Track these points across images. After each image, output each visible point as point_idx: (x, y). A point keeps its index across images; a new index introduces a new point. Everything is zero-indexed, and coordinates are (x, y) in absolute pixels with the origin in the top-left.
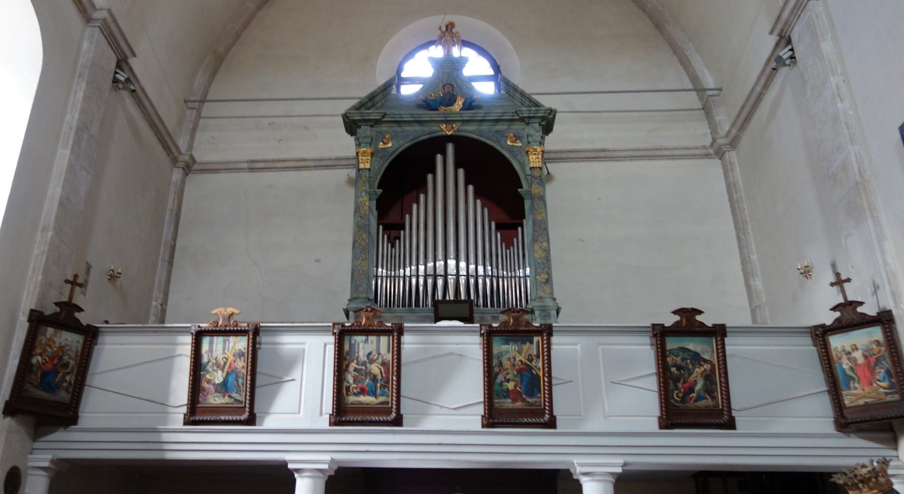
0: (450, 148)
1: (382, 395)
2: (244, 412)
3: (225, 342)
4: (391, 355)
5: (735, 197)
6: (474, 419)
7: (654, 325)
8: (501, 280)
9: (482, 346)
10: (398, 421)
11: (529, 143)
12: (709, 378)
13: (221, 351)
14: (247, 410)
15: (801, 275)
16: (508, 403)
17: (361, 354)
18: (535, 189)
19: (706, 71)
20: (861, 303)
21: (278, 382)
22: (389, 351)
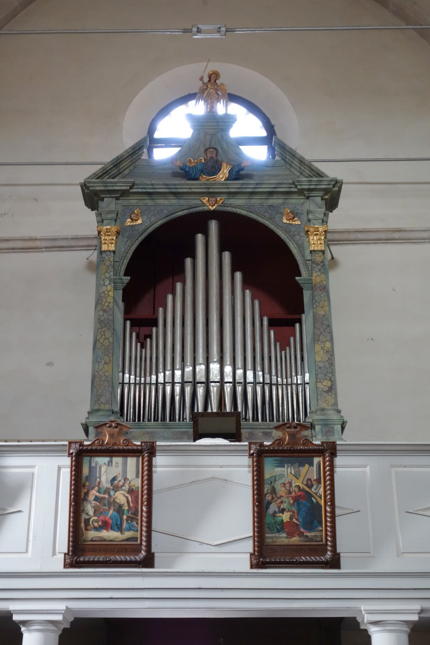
1: (129, 529)
4: (140, 480)
8: (274, 388)
11: (309, 220)
17: (103, 479)
18: (317, 278)
22: (137, 476)
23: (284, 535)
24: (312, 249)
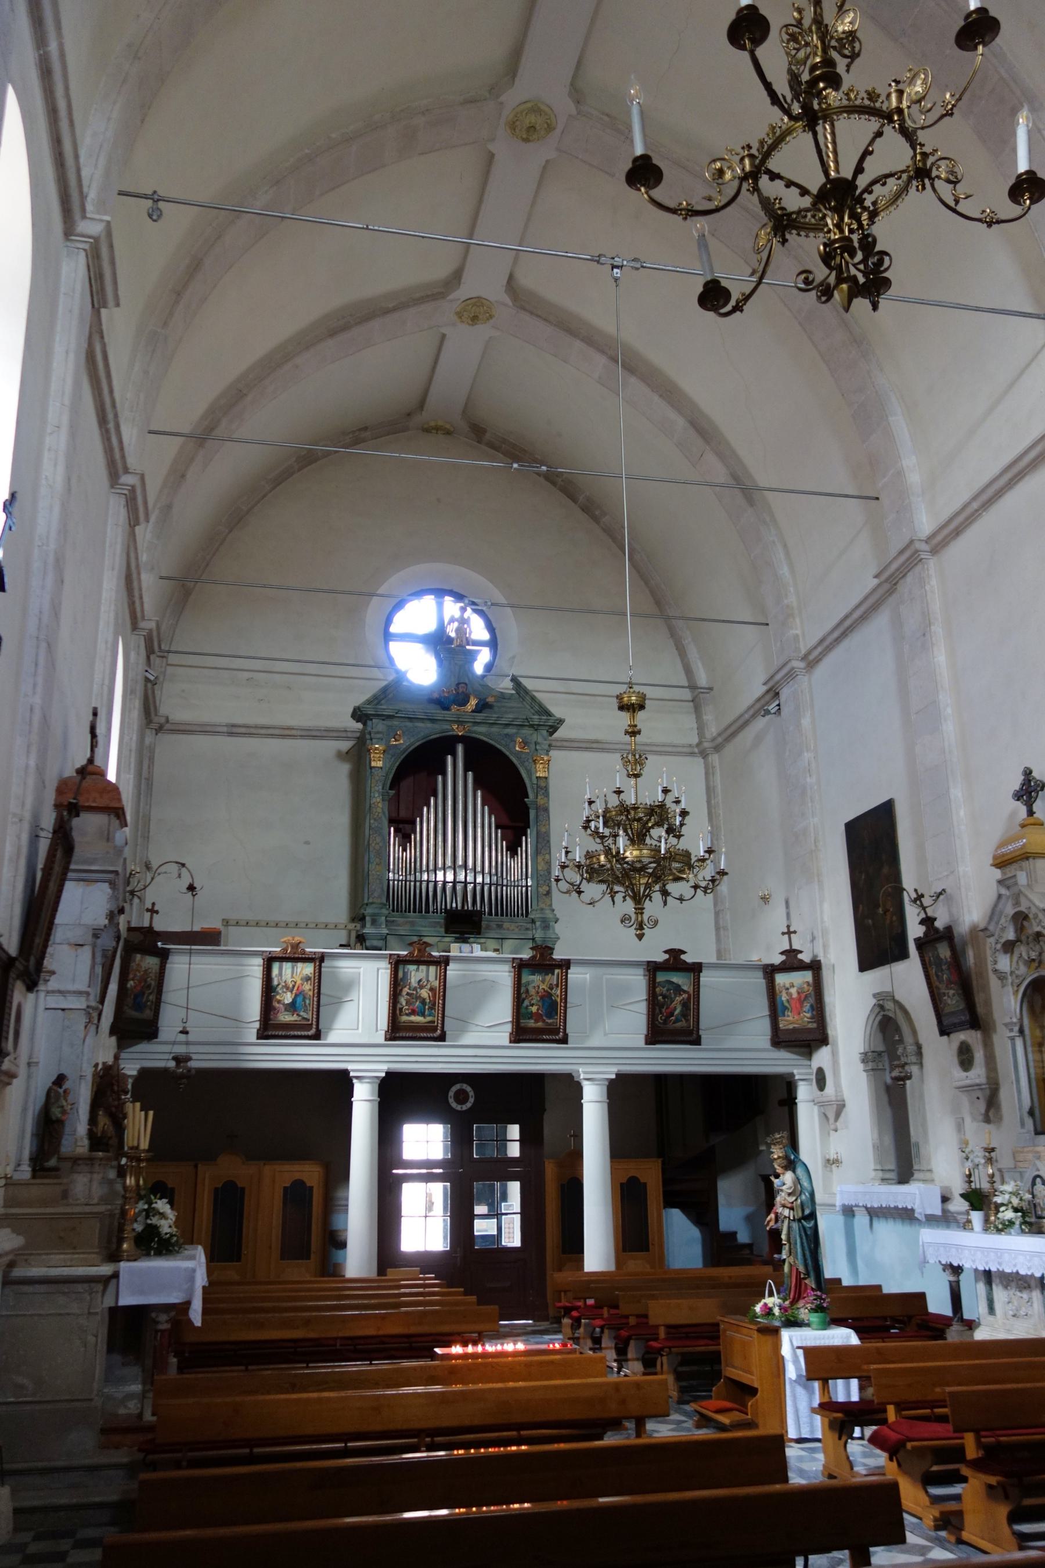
0: (460, 749)
1: (430, 1015)
2: (311, 1029)
3: (293, 968)
4: (438, 982)
5: (713, 802)
6: (503, 1036)
7: (649, 962)
8: (504, 888)
9: (512, 974)
10: (442, 1038)
11: (536, 750)
12: (685, 1005)
13: (290, 976)
14: (314, 1026)
15: (767, 129)
16: (531, 1023)
17: (413, 980)
18: (541, 801)
19: (700, 665)
20: (801, 952)
21: (338, 1003)
22: (436, 979)
23: (533, 1021)
24: (538, 775)
